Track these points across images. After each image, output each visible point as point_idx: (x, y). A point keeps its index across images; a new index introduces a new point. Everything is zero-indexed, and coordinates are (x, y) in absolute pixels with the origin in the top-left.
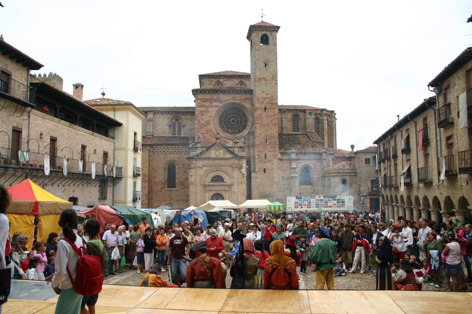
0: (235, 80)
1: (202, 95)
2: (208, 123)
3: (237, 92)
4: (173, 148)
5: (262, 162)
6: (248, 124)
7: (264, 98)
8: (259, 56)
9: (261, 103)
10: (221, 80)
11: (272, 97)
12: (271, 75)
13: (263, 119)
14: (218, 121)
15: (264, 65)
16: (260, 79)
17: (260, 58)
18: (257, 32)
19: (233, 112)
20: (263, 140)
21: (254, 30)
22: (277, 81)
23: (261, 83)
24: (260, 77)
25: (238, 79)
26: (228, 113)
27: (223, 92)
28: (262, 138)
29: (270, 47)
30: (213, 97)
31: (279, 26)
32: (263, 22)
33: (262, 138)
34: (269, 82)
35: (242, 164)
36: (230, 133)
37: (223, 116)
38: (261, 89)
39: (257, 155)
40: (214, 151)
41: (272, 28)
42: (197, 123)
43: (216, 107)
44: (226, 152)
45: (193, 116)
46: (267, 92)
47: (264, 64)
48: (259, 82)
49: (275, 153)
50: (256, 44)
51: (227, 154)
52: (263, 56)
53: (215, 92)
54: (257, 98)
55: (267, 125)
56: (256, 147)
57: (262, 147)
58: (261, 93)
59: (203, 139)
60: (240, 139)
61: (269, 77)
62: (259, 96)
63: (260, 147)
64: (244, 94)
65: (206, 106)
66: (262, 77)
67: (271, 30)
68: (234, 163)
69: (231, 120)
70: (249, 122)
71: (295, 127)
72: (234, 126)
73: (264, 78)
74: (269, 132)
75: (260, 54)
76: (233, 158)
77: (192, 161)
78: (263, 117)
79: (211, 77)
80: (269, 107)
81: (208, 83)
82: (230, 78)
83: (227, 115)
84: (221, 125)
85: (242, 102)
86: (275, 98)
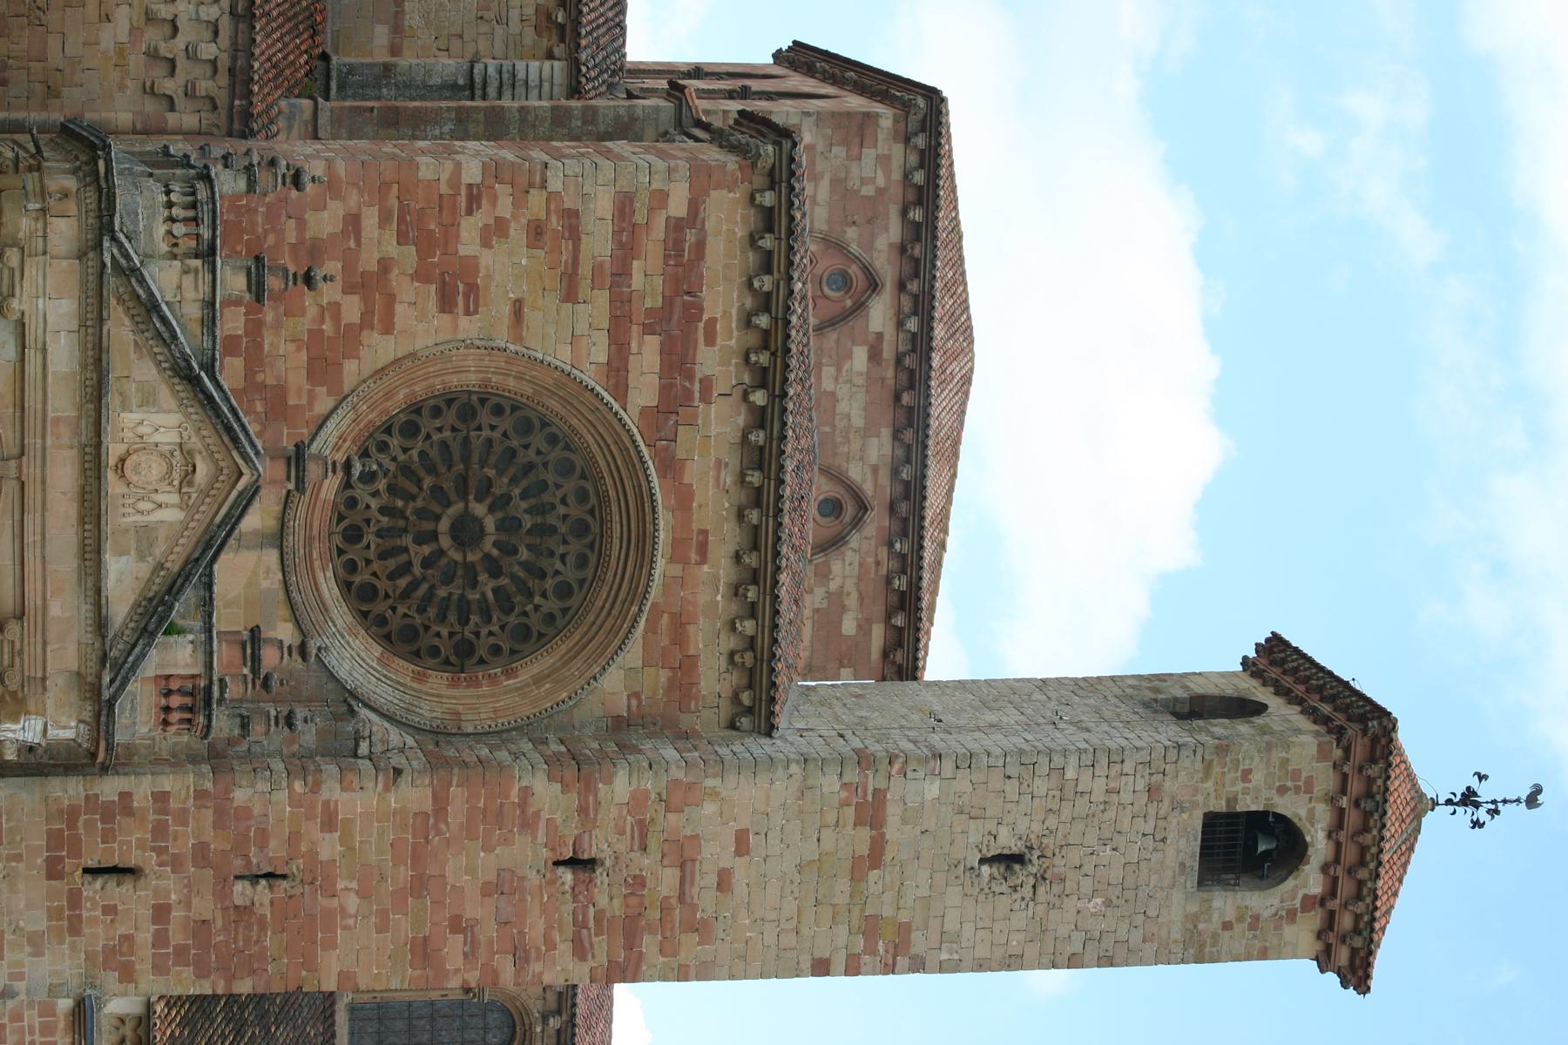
0: (880, 448)
1: (740, 232)
3: (754, 577)
4: (208, 50)
5: (54, 839)
6: (438, 681)
7: (683, 857)
8: (1098, 796)
9: (643, 828)
10: (879, 314)
11: (701, 929)
12: (904, 917)
13: (487, 848)
14: (472, 380)
15: (1008, 842)
16: (871, 813)
17: (1082, 806)
18: (1326, 780)
19: (563, 529)
20: (276, 848)
21: (1347, 751)
22: (852, 969)
23: (831, 818)
24: (893, 812)
25: (884, 478)
26: (551, 478)
27: (758, 437)
28: (294, 838)
29: (1177, 897)
30: (710, 340)
31: (1373, 984)
32: (1418, 818)
33: (294, 838)
34: (842, 899)
35: (42, 713)
36: (352, 503)
37: (526, 427)
38: (777, 820)
39: (125, 796)
40: (168, 438)
41: (1357, 917)
42: (454, 182)
43: (617, 371)
44: (159, 550)
45: (529, 35)
46: (740, 880)
47: (1016, 847)
48: (845, 803)
49: (143, 967)
50: (1216, 769)
51: (145, 569)
52: (1091, 839)
53: (763, 359)
54: (690, 787)
55: (419, 886)
56: (209, 785)
57: (209, 834)
58: (734, 826)
59: (291, 237)
60: (284, 611)
61: (888, 897)
62: (709, 808)
63: (208, 816)
64: (729, 642)
65: (622, 273)
66: (892, 829)
67: (1334, 904)
68: (52, 633)
69: (479, 509)
70: (454, 684)
71: (400, 1025)
72: (420, 540)
73: (877, 849)
74: (352, 903)
75: (1111, 814)
76: (100, 624)
77: (72, 207)
78: (506, 842)
79: (899, 621)
80: (602, 901)
81: (854, 183)
82: (897, 398)
83: (530, 467)
84: (437, 412)
85: (652, 628)
86: (683, 956)
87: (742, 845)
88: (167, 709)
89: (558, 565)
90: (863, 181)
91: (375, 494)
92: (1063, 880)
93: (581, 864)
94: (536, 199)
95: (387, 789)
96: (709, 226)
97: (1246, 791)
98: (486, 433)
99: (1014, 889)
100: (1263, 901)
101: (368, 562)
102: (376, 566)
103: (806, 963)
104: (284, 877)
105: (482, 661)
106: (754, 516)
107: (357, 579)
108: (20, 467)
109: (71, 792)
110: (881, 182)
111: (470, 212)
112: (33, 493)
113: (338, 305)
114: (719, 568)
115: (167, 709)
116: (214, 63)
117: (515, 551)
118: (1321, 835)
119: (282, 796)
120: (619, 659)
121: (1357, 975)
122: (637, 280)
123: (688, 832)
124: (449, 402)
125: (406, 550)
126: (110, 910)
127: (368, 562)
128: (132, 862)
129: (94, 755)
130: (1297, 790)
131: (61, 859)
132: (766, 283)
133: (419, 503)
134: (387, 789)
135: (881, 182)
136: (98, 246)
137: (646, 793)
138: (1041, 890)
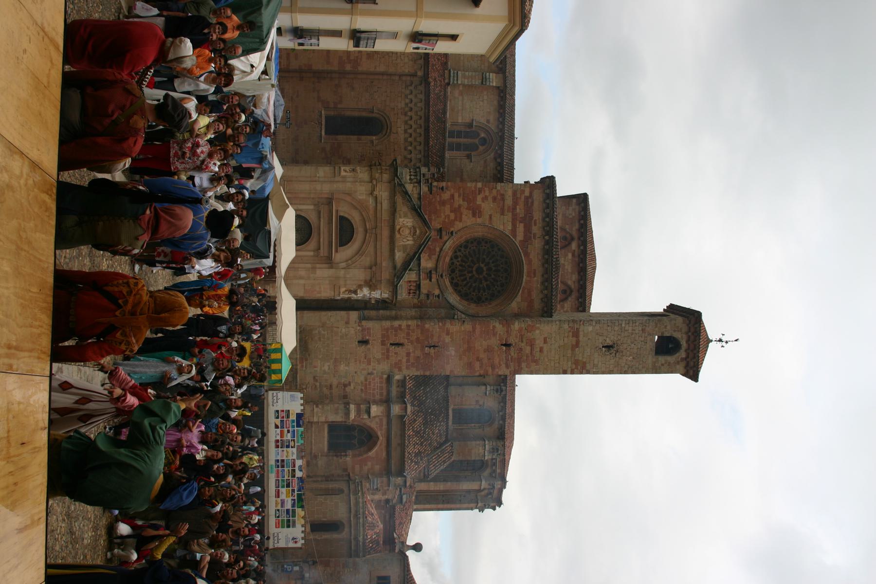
0: (575, 277)
2: (476, 212)
3: (547, 280)
5: (383, 336)
6: (473, 306)
8: (630, 331)
9: (522, 337)
10: (574, 246)
12: (584, 360)
15: (609, 342)
16: (576, 334)
20: (435, 339)
21: (690, 321)
23: (566, 335)
24: (581, 333)
27: (547, 247)
29: (650, 357)
30: (535, 225)
31: (699, 380)
34: (569, 355)
35: (381, 289)
36: (453, 263)
39: (400, 326)
40: (410, 224)
41: (694, 362)
42: (475, 187)
46: (545, 349)
47: (611, 343)
48: (570, 331)
49: (404, 367)
50: (659, 325)
51: (405, 255)
52: (629, 341)
56: (419, 323)
60: (437, 287)
62: (537, 332)
64: (541, 296)
65: (514, 209)
66: (581, 338)
67: (688, 360)
69: (482, 265)
72: (469, 273)
75: (633, 336)
76: (395, 267)
77: (388, 172)
79: (582, 222)
80: (513, 354)
82: (579, 265)
87: (545, 341)
88: (410, 290)
89: (501, 279)
90: (570, 215)
91: (458, 261)
92: (622, 352)
93: (507, 345)
94: (494, 191)
95: (461, 325)
96: (534, 198)
97: (666, 331)
98: (484, 248)
99: (611, 354)
100: (670, 359)
101: (457, 277)
102: (458, 278)
103: (561, 371)
104: (437, 346)
105: (483, 302)
106: (546, 266)
107: (454, 281)
108: (376, 231)
109: (387, 324)
110: (574, 215)
111: (479, 194)
112: (379, 236)
113: (449, 215)
114: (538, 279)
115: (410, 290)
116: (420, 151)
117: (491, 276)
118: (684, 342)
119: (437, 326)
120: (515, 300)
121: (695, 378)
122: (518, 210)
123: (532, 337)
124: (475, 240)
125: (465, 275)
126: (396, 353)
127: (457, 277)
128: (401, 342)
129: (392, 301)
130: (678, 331)
131: (384, 341)
132: (548, 211)
133: (468, 264)
134: (461, 325)
135: (574, 215)
136: (394, 180)
137: (522, 328)
138: (617, 354)
